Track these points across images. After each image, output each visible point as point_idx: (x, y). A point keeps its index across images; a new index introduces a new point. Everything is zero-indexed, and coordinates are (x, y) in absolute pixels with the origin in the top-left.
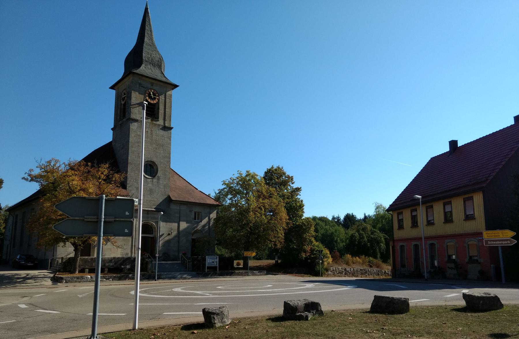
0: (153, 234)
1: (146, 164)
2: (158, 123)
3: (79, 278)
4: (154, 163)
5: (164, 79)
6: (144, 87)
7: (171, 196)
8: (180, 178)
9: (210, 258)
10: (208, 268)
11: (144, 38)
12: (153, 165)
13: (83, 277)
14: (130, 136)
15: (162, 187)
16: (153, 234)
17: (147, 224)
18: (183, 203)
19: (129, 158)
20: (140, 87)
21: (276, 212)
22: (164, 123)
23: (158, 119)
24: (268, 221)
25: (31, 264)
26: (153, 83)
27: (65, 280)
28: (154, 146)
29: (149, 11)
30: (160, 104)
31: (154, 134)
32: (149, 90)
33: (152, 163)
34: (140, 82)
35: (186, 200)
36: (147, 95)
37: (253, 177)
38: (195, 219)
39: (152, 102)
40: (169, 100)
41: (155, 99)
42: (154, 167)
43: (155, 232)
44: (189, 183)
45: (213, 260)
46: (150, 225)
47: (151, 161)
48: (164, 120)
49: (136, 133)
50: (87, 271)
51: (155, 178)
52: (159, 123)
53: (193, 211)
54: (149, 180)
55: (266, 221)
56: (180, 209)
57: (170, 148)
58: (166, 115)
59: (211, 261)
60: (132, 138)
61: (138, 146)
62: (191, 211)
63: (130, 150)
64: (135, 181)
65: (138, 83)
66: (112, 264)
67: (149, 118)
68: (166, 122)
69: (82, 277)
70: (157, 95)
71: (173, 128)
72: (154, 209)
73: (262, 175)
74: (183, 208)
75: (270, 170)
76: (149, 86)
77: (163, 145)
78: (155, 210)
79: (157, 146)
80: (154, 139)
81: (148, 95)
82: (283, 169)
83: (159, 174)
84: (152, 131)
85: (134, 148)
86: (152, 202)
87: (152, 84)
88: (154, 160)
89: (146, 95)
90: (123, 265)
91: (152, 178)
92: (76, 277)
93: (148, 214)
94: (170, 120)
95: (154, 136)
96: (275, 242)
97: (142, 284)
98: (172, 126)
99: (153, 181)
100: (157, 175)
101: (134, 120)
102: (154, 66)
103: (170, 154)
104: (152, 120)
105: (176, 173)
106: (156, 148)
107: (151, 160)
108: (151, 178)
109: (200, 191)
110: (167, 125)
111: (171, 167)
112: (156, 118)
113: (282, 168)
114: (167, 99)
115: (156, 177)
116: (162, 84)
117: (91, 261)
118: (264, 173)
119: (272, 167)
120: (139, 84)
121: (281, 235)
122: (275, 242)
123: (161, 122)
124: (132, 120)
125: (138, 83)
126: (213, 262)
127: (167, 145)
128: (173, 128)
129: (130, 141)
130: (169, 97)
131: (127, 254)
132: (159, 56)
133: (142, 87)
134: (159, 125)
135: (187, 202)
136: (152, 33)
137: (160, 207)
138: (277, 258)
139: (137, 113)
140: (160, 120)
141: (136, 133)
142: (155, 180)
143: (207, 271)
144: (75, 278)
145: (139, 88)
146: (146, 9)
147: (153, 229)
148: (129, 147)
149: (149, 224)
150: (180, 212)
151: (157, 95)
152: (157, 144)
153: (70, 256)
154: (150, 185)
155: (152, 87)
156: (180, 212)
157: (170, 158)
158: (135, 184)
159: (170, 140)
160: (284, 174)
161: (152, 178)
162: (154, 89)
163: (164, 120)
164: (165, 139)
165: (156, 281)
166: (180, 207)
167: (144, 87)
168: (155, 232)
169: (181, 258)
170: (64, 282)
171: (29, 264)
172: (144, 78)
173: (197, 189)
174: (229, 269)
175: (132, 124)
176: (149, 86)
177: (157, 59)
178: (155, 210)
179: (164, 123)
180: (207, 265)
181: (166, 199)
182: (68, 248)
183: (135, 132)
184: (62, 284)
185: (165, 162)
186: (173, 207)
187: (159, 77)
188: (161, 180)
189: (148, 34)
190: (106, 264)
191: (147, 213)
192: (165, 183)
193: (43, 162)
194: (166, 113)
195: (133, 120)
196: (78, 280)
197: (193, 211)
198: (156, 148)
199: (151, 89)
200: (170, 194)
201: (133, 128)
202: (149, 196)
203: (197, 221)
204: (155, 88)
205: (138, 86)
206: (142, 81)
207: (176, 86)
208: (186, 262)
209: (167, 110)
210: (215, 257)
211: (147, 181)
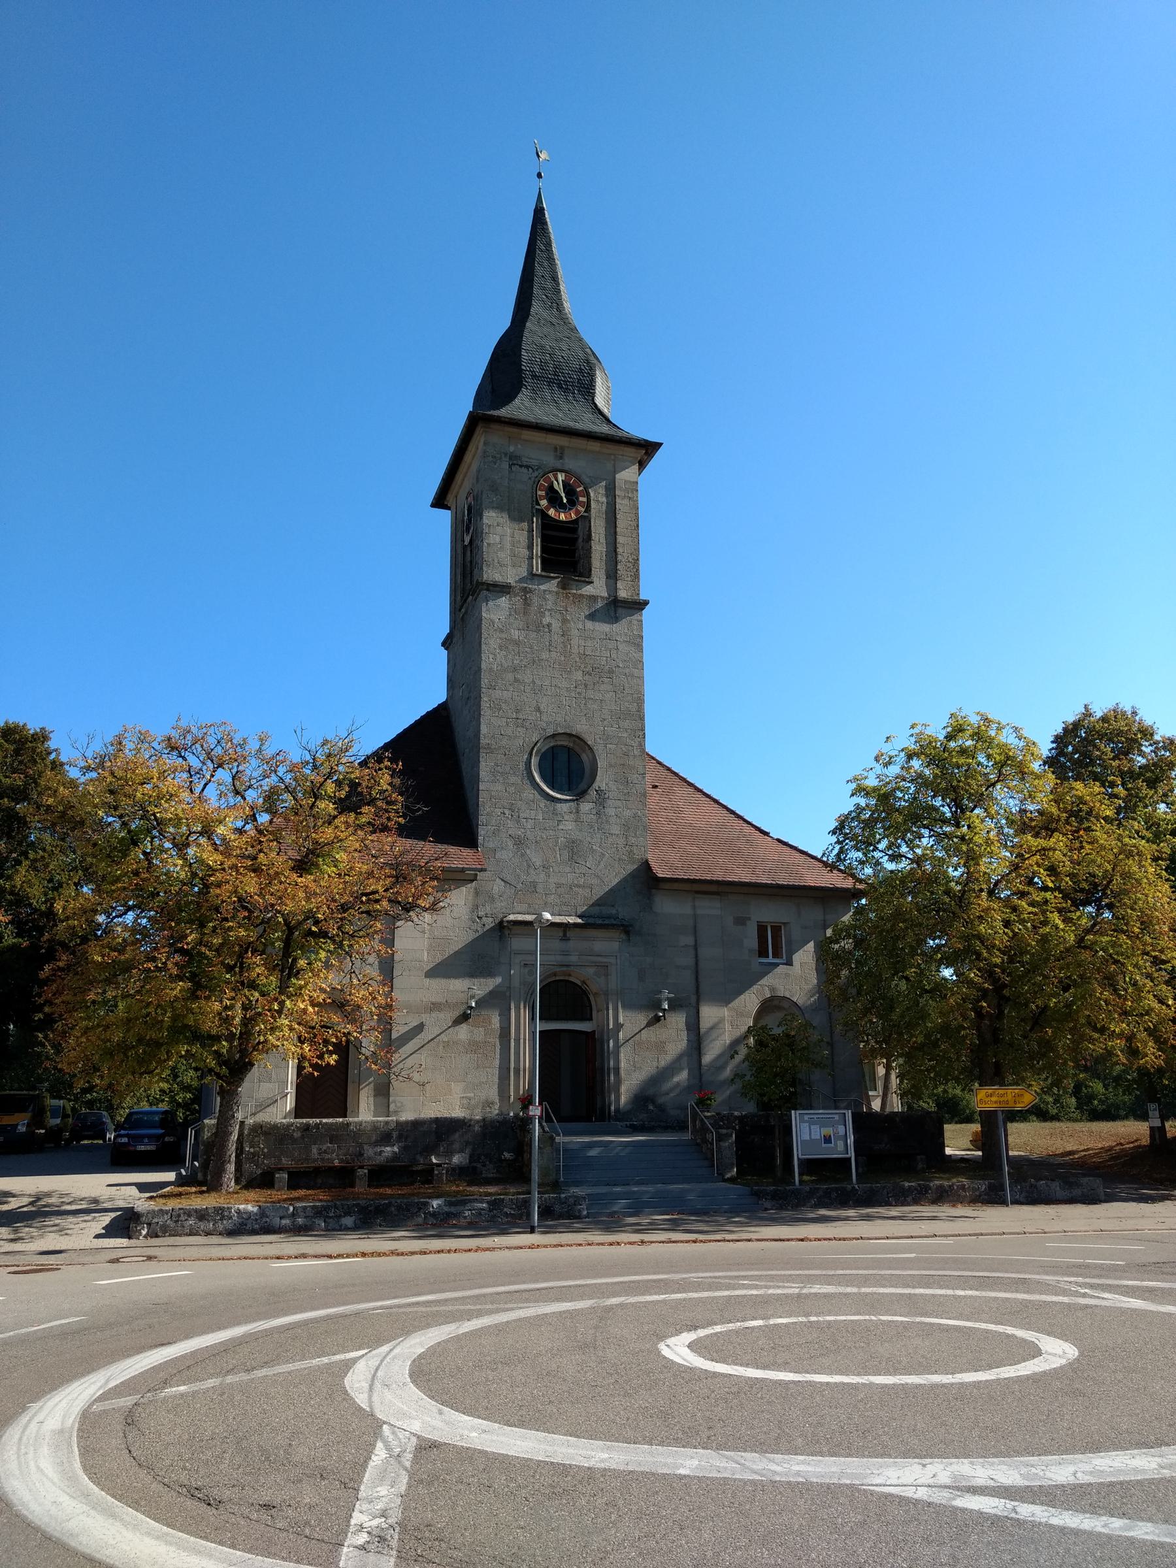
0: (591, 1019)
1: (553, 748)
2: (588, 590)
3: (208, 1215)
4: (578, 738)
5: (605, 429)
6: (527, 467)
7: (652, 863)
8: (699, 795)
9: (811, 1122)
10: (810, 1166)
11: (530, 305)
12: (577, 749)
13: (226, 1214)
14: (483, 646)
15: (616, 830)
16: (591, 1019)
17: (567, 978)
18: (713, 888)
19: (484, 729)
20: (514, 468)
21: (1114, 886)
22: (612, 589)
23: (589, 576)
24: (1082, 939)
25: (149, 1148)
26: (562, 448)
27: (149, 1224)
28: (579, 675)
29: (547, 216)
30: (592, 521)
31: (575, 632)
32: (551, 475)
33: (574, 742)
34: (512, 449)
35: (718, 875)
36: (543, 493)
37: (978, 735)
38: (763, 952)
39: (562, 517)
40: (626, 501)
41: (572, 503)
42: (584, 757)
43: (598, 1011)
44: (733, 812)
45: (828, 1131)
46: (579, 983)
47: (570, 735)
48: (612, 575)
49: (504, 636)
50: (284, 1178)
51: (587, 797)
52: (592, 590)
53: (749, 919)
54: (564, 807)
55: (1071, 938)
56: (695, 916)
57: (641, 678)
58: (619, 557)
59: (817, 1132)
60: (491, 656)
61: (516, 680)
62: (741, 921)
63: (485, 698)
64: (507, 812)
65: (506, 454)
66: (388, 1149)
67: (552, 575)
68: (620, 585)
69: (222, 1209)
70: (581, 488)
71: (646, 603)
72: (580, 917)
73: (1045, 747)
74: (709, 908)
75: (1076, 725)
76: (549, 460)
77: (611, 672)
78: (579, 921)
79: (590, 675)
80: (575, 650)
81: (547, 494)
82: (1137, 718)
83: (601, 781)
84: (565, 621)
85: (499, 689)
86: (580, 891)
87: (560, 453)
88: (581, 727)
89: (539, 493)
90: (438, 1156)
91: (574, 798)
92: (196, 1211)
93: (565, 938)
94: (636, 576)
95: (575, 642)
96: (1130, 1038)
97: (449, 1251)
98: (643, 596)
99: (578, 812)
100: (596, 785)
101: (498, 589)
102: (566, 390)
103: (640, 701)
104: (564, 586)
105: (684, 780)
106: (586, 686)
107: (568, 731)
108: (570, 800)
109: (779, 841)
110: (623, 594)
111: (650, 749)
112: (581, 575)
113: (1134, 713)
114: (618, 500)
115: (592, 793)
116: (595, 446)
117: (303, 1137)
118: (1052, 742)
119: (1087, 714)
120: (510, 458)
121: (1156, 1005)
122: (1130, 1038)
123: (598, 587)
124: (488, 590)
125: (506, 454)
126: (827, 1140)
127: (627, 671)
128: (646, 603)
129: (483, 666)
130: (627, 490)
131: (488, 1104)
132: (581, 354)
133: (521, 466)
134: (593, 598)
135: (718, 883)
136: (558, 285)
137: (614, 912)
138: (1157, 1113)
139: (508, 561)
140: (595, 578)
141: (504, 636)
142: (586, 807)
143: (800, 1181)
144: (189, 1215)
145: (511, 471)
146: (539, 213)
147: (592, 998)
148: (483, 690)
149: (572, 979)
150: (695, 927)
151: (581, 488)
152: (589, 669)
153: (267, 1119)
154: (569, 825)
155: (558, 464)
156: (695, 927)
157: (642, 719)
158: (510, 824)
159: (639, 647)
160: (1147, 733)
161: (574, 798)
162: (566, 468)
163: (612, 575)
164: (620, 647)
165: (532, 1231)
166: (694, 907)
167: (527, 467)
168: (598, 1011)
169: (694, 1121)
170: (144, 1232)
171: (142, 1148)
172: (527, 434)
173: (766, 834)
174: (920, 1166)
175: (491, 603)
176: (549, 460)
177: (576, 364)
178: (579, 921)
179: (612, 589)
180: (798, 1154)
181: (633, 875)
182: (256, 1086)
183: (501, 631)
184: (133, 1242)
185: (625, 735)
186: (667, 906)
187: (587, 423)
188: (610, 802)
189: (544, 289)
190: (366, 1147)
191: (561, 934)
192: (628, 813)
193: (97, 748)
194: (620, 550)
195: (491, 588)
196: (202, 1225)
197: (749, 919)
198: (586, 686)
199: (555, 471)
200: (649, 857)
201: (492, 616)
202: (568, 869)
203: (771, 959)
204: (570, 463)
205: (505, 466)
206: (519, 446)
207: (647, 449)
208: (708, 1136)
209: (620, 539)
210: (837, 1117)
211: (555, 813)
